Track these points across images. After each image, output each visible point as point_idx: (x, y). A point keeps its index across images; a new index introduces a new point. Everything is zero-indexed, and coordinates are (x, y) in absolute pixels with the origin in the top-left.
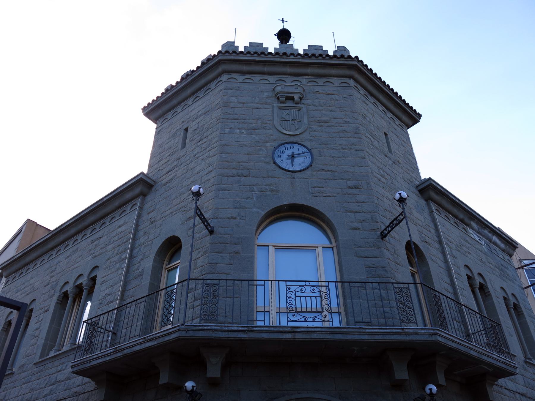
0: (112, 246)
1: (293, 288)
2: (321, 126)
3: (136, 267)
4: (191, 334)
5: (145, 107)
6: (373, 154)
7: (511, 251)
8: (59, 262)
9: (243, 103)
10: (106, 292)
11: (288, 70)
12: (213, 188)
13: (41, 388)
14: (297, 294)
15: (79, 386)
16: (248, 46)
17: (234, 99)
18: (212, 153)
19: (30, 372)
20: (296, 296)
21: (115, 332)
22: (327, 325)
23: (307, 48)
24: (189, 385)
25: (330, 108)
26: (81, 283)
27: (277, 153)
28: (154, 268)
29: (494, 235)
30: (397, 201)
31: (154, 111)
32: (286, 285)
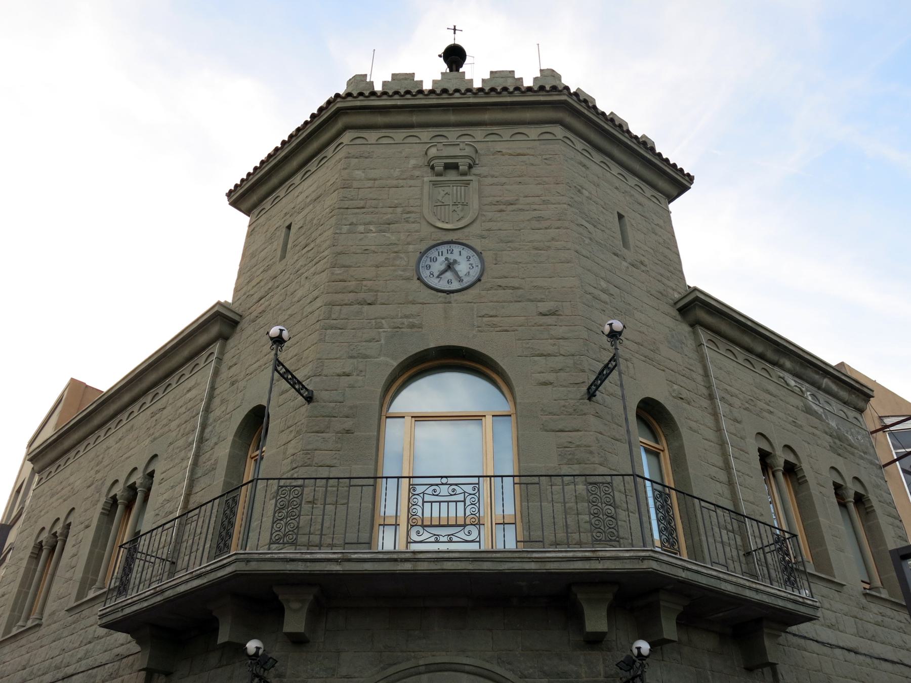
0: (177, 422)
1: (420, 489)
2: (501, 211)
3: (208, 455)
4: (253, 566)
5: (231, 191)
6: (588, 255)
7: (861, 404)
8: (109, 448)
9: (375, 180)
10: (166, 496)
11: (452, 118)
12: (318, 326)
13: (75, 648)
14: (427, 498)
15: (122, 645)
16: (390, 80)
17: (359, 174)
18: (320, 267)
19: (62, 622)
20: (424, 502)
21: (174, 560)
22: (474, 547)
23: (487, 76)
24: (252, 646)
25: (519, 179)
26: (135, 483)
27: (425, 261)
28: (231, 457)
29: (825, 377)
30: (608, 336)
31: (248, 195)
32: (410, 485)
